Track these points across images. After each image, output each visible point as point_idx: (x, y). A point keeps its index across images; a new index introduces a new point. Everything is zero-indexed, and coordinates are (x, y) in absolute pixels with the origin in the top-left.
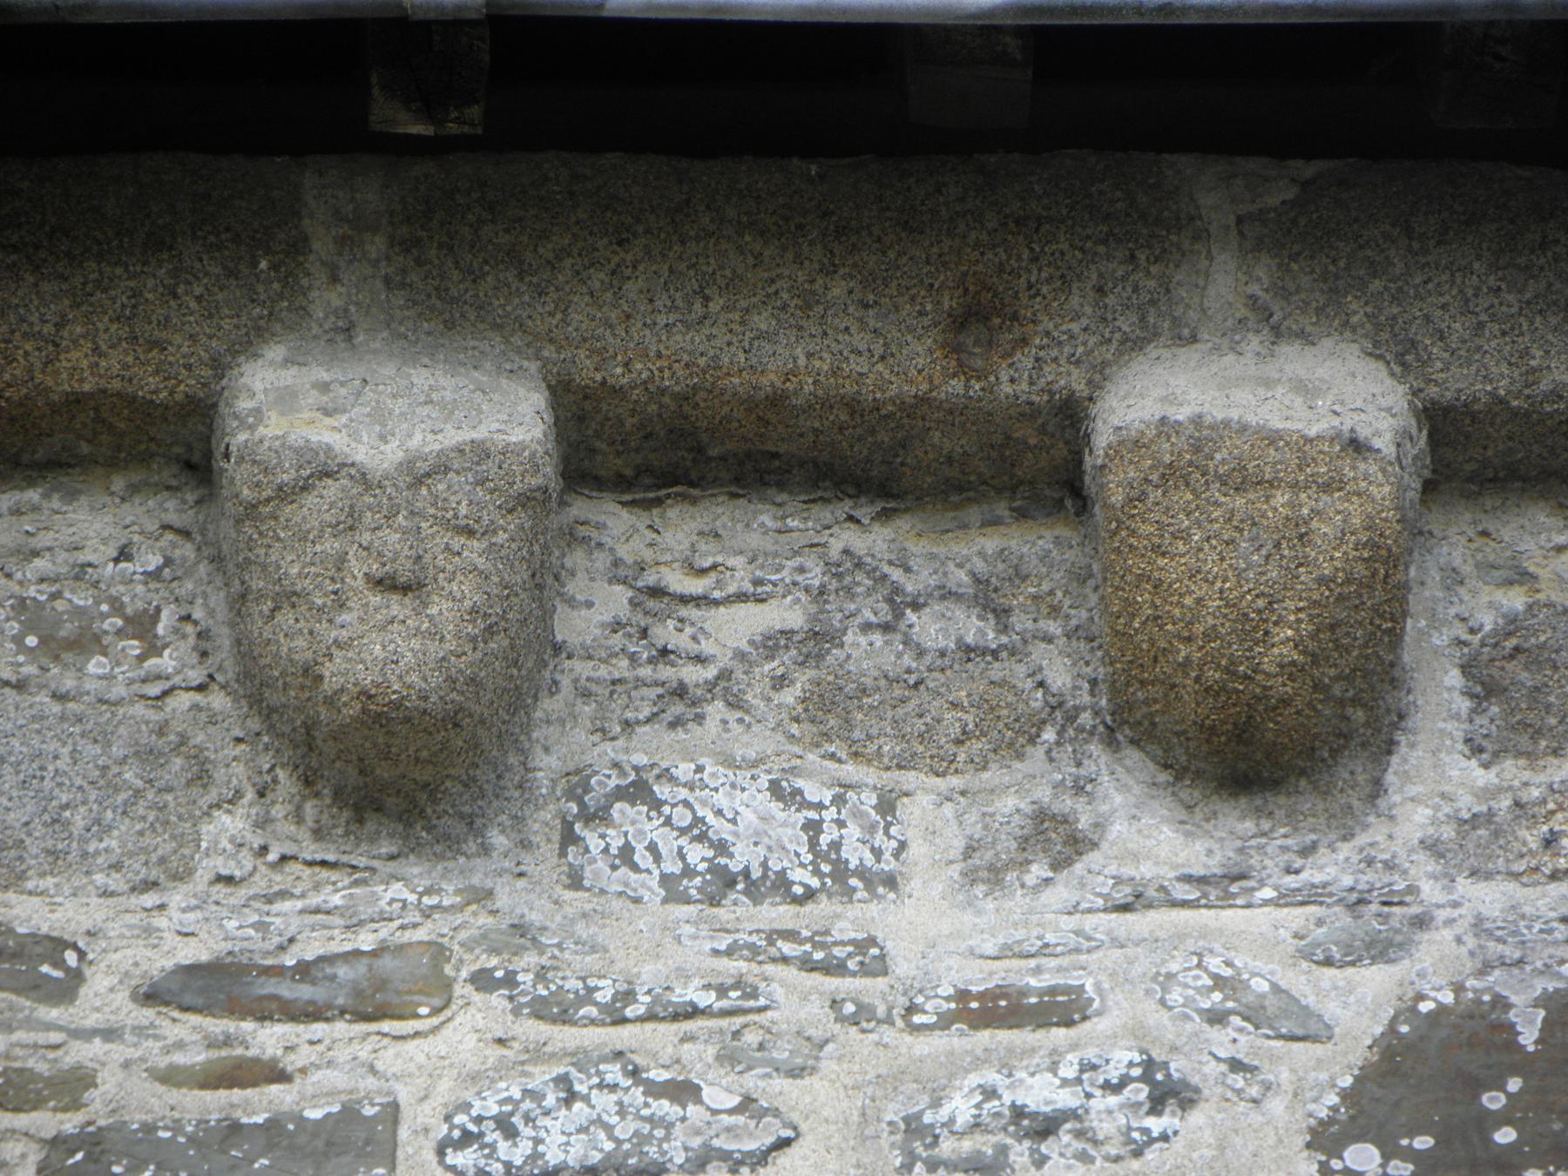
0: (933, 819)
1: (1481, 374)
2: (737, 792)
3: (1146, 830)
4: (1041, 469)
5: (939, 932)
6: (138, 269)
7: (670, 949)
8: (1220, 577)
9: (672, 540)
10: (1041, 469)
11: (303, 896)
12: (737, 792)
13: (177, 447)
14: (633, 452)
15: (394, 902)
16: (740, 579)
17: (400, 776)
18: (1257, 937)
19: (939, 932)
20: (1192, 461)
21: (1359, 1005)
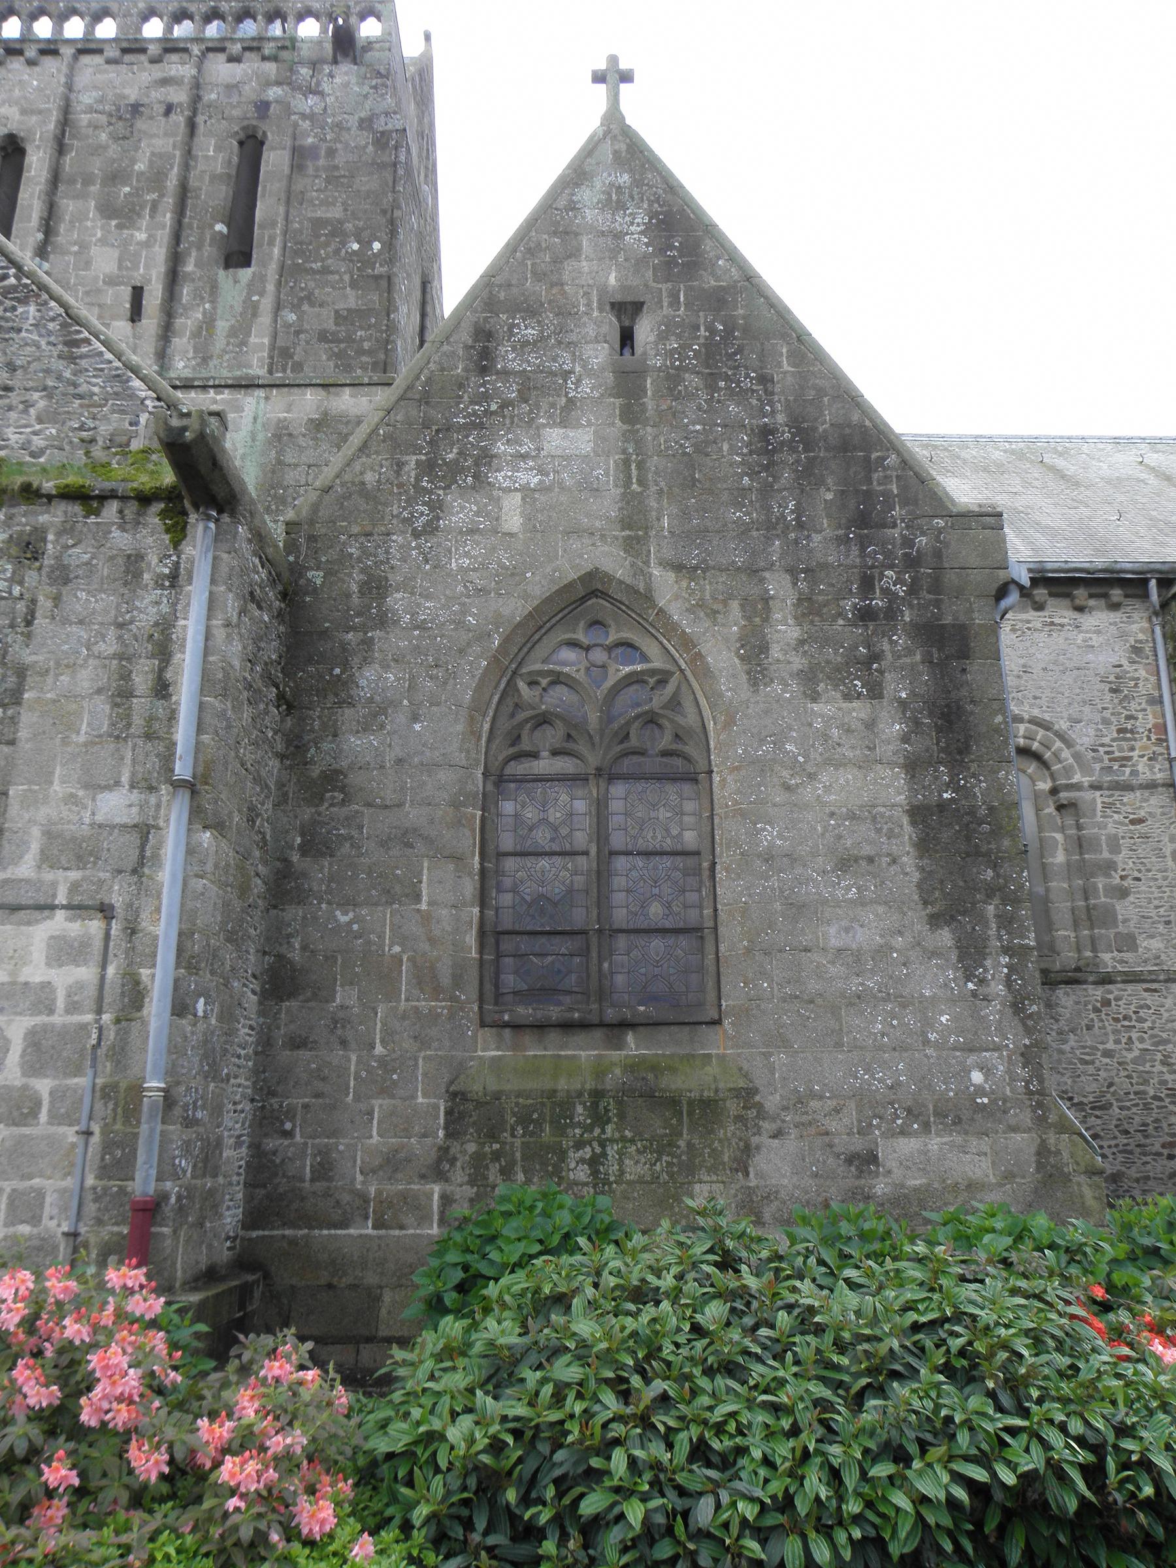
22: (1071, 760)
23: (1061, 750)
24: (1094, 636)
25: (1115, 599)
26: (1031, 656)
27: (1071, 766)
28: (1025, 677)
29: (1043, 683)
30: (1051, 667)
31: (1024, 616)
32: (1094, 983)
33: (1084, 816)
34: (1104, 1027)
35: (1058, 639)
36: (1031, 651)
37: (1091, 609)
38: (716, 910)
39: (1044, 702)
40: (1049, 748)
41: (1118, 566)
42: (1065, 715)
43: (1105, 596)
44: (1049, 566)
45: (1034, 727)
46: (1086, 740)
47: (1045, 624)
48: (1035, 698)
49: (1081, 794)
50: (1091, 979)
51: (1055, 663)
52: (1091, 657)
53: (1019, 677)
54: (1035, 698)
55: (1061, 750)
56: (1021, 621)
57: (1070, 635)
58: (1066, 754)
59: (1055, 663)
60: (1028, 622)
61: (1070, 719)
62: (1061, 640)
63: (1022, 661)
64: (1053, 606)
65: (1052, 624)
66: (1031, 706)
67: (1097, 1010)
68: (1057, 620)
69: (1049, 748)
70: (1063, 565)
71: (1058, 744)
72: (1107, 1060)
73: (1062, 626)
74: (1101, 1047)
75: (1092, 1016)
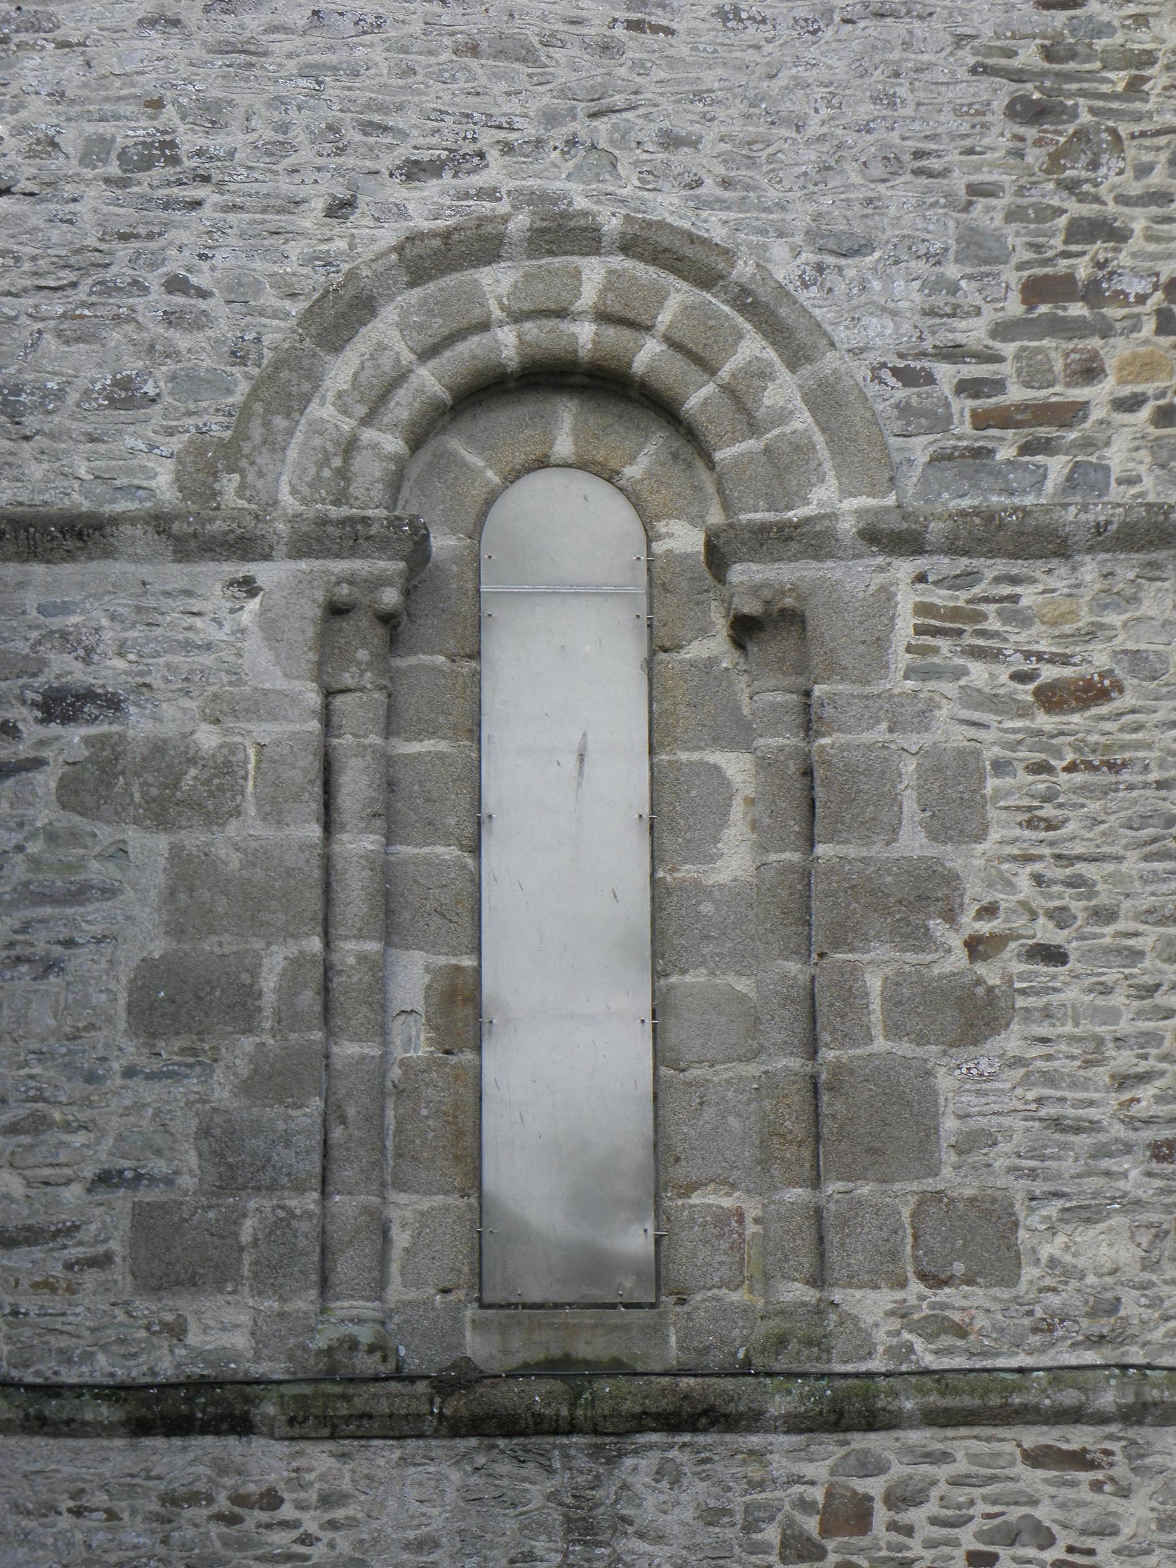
22: (803, 421)
27: (802, 448)
28: (636, 47)
29: (710, 78)
32: (796, 1424)
33: (833, 670)
39: (705, 161)
42: (800, 217)
45: (645, 272)
48: (671, 141)
49: (832, 570)
55: (763, 374)
58: (783, 392)
66: (651, 177)
71: (753, 347)
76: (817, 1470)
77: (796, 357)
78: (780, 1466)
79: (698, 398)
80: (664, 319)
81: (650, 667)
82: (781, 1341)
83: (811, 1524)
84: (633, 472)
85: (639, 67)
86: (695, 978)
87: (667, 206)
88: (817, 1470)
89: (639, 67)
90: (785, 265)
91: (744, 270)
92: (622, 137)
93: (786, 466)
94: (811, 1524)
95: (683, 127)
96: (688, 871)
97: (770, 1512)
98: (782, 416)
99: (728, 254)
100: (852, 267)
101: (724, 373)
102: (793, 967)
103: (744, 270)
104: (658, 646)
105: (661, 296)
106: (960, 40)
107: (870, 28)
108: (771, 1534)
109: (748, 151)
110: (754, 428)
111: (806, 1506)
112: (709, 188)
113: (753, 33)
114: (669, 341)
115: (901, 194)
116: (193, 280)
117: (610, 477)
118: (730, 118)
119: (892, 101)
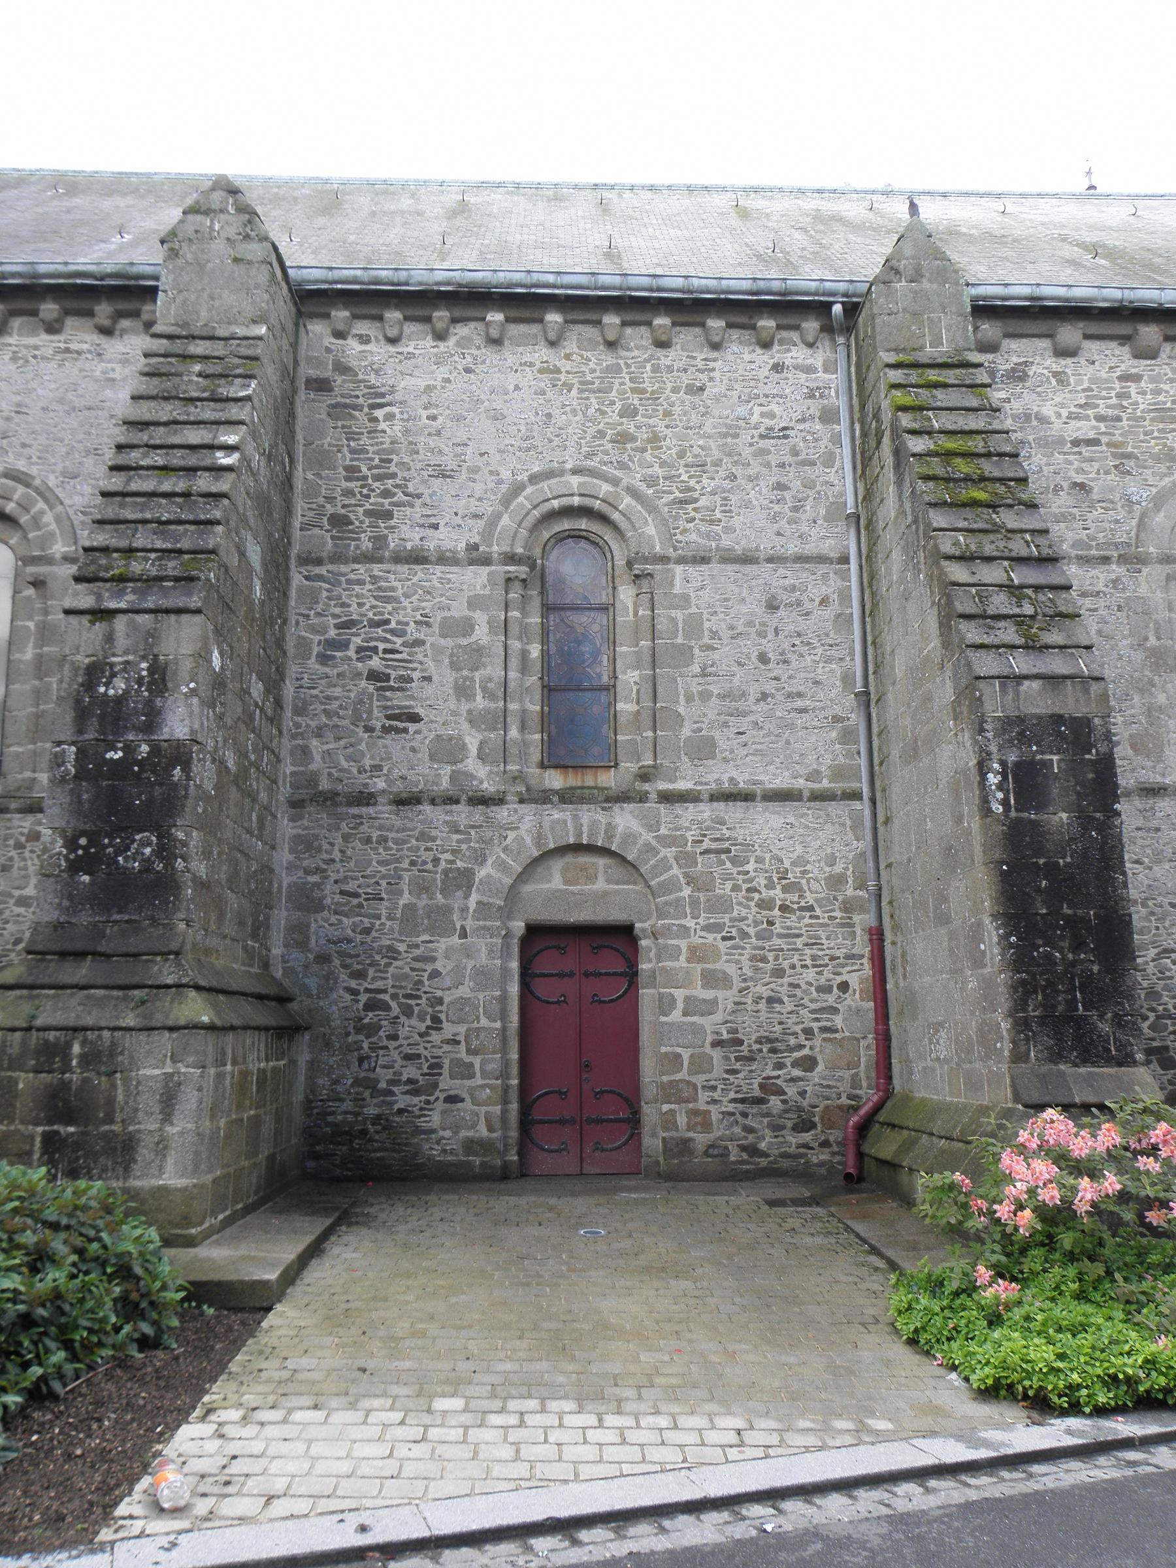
0: (746, 350)
1: (569, 317)
2: (735, 348)
3: (759, 351)
4: (753, 327)
5: (747, 357)
6: (41, 1312)
7: (732, 358)
8: (764, 335)
9: (731, 331)
10: (753, 327)
11: (1101, 1411)
12: (735, 348)
13: (702, 325)
14: (730, 326)
15: (715, 354)
16: (735, 334)
17: (716, 346)
18: (765, 358)
19: (747, 357)
20: (763, 327)
21: (771, 362)
22: (53, 526)
23: (42, 512)
24: (118, 367)
25: (440, 325)
26: (30, 391)
27: (52, 534)
28: (17, 418)
29: (37, 427)
30: (54, 406)
31: (32, 341)
32: (20, 811)
33: (53, 597)
34: (26, 868)
35: (71, 370)
36: (33, 385)
37: (124, 331)
38: (801, 559)
39: (34, 452)
40: (26, 510)
41: (134, 270)
42: (59, 468)
43: (428, 320)
44: (42, 269)
45: (11, 483)
46: (78, 500)
47: (58, 351)
48: (24, 446)
49: (55, 569)
50: (13, 806)
51: (61, 401)
52: (108, 393)
53: (8, 419)
54: (24, 446)
55: (42, 512)
56: (27, 347)
57: (87, 366)
58: (48, 518)
59: (61, 401)
60: (36, 348)
61: (64, 474)
62: (75, 371)
63: (16, 399)
64: (74, 328)
65: (67, 350)
66: (18, 456)
67: (19, 846)
68: (74, 346)
69: (26, 510)
70: (61, 268)
71: (41, 505)
72: (22, 910)
73: (79, 353)
74: (16, 893)
75: (13, 853)
76: (27, 824)
77: (51, 507)
78: (16, 823)
79: (24, 519)
80: (16, 497)
81: (13, 598)
82: (19, 788)
83: (23, 839)
84: (12, 542)
85: (18, 425)
86: (17, 686)
87: (21, 465)
88: (27, 824)
89: (18, 425)
90: (52, 481)
91: (37, 482)
92: (10, 445)
93: (49, 538)
94: (23, 839)
95: (28, 441)
96: (17, 656)
97: (11, 836)
98: (47, 525)
99: (33, 477)
100: (72, 482)
101: (32, 512)
102: (36, 682)
103: (37, 482)
104: (16, 591)
105: (15, 490)
106: (112, 416)
107: (86, 413)
108: (11, 842)
109: (46, 449)
110: (39, 529)
111: (22, 834)
112: (35, 459)
113: (52, 414)
114: (19, 504)
115: (89, 461)
116: (135, 545)
117: (6, 543)
118: (42, 439)
119: (89, 434)
